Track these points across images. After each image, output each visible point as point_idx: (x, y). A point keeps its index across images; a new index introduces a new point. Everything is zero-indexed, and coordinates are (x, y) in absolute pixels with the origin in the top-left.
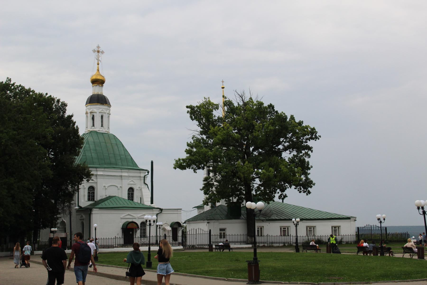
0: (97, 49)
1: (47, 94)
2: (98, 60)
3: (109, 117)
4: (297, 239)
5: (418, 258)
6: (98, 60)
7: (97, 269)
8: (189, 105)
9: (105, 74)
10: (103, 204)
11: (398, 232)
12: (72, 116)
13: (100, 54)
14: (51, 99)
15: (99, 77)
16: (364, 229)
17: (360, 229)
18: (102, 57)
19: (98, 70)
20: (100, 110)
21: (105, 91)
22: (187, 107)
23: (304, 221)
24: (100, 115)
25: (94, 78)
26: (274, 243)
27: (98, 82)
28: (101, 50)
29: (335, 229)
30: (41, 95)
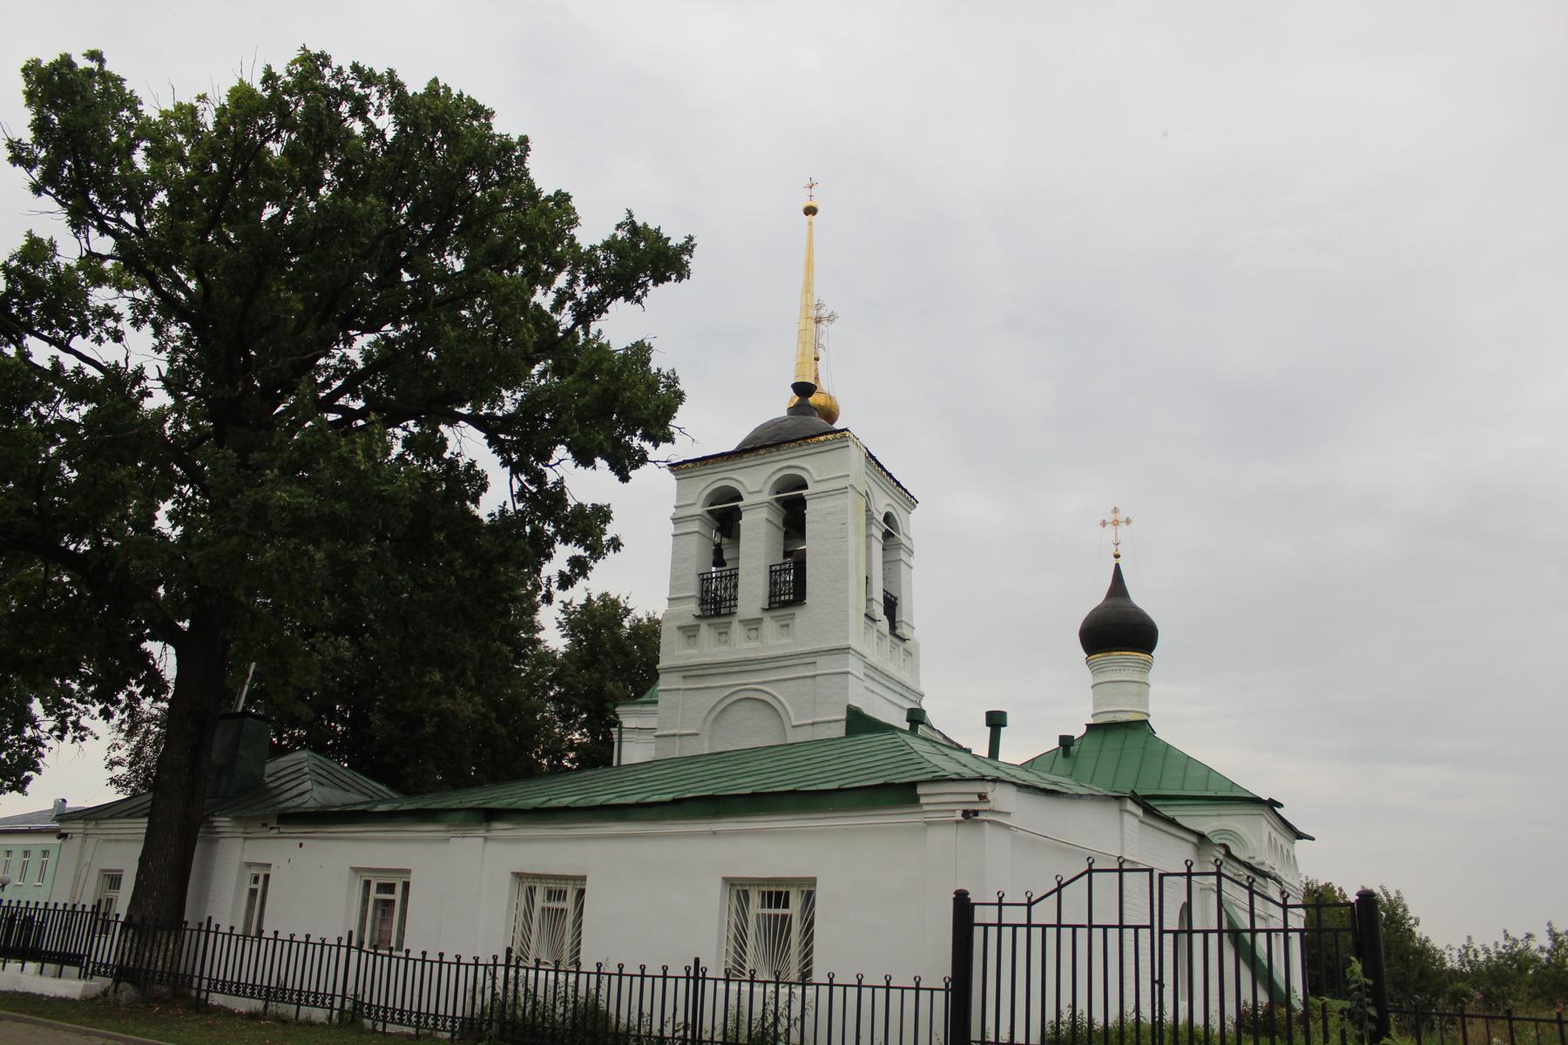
6: (817, 346)
13: (822, 327)
16: (1044, 913)
17: (980, 915)
23: (500, 829)
28: (824, 313)
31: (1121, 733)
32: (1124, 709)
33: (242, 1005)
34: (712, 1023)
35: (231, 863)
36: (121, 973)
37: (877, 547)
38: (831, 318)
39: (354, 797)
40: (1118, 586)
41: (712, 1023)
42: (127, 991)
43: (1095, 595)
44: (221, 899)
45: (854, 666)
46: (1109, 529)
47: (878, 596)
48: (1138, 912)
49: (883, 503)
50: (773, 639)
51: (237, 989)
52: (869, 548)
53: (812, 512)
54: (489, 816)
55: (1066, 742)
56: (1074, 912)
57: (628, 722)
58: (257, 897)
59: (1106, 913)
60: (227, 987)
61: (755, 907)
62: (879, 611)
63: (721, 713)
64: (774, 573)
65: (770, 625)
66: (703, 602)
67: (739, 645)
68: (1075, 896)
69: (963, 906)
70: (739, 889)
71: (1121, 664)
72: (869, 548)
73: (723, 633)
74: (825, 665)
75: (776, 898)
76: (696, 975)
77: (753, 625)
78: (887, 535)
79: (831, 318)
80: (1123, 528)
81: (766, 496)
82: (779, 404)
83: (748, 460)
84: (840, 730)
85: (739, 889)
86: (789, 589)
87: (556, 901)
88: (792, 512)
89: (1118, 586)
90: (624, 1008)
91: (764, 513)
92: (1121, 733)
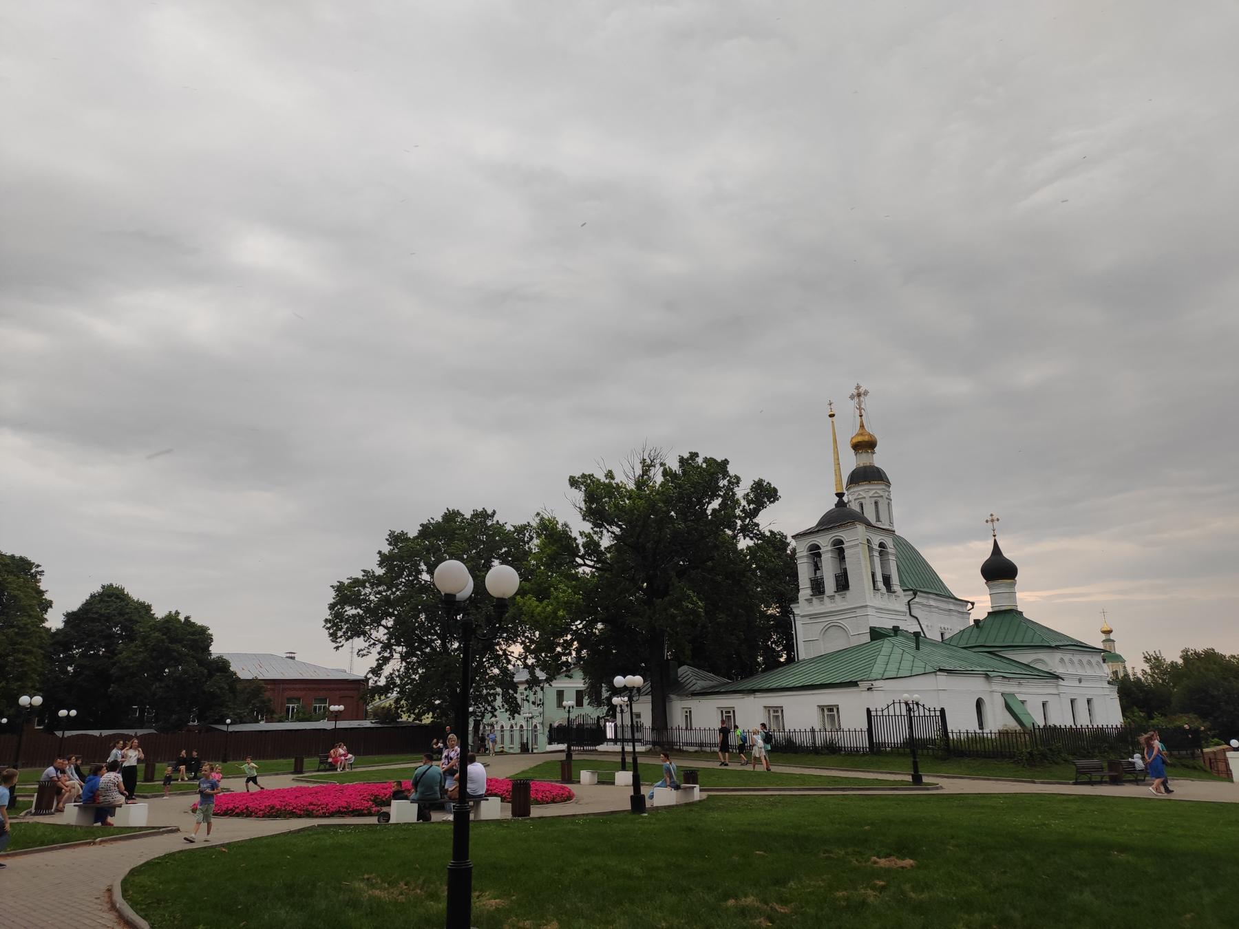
0: (855, 392)
1: (764, 494)
2: (860, 409)
3: (889, 504)
4: (814, 738)
5: (514, 814)
6: (860, 409)
7: (674, 792)
8: (577, 474)
9: (873, 429)
10: (1043, 655)
11: (410, 756)
12: (380, 552)
14: (451, 516)
15: (866, 438)
17: (873, 713)
18: (867, 402)
19: (862, 426)
20: (871, 493)
21: (879, 459)
22: (573, 482)
23: (758, 695)
24: (873, 500)
25: (855, 441)
26: (706, 745)
27: (865, 445)
28: (862, 390)
29: (830, 711)
30: (13, 557)
31: (1005, 616)
32: (1005, 605)
33: (692, 749)
34: (818, 743)
35: (678, 708)
36: (654, 743)
37: (877, 560)
38: (866, 393)
39: (712, 683)
40: (996, 550)
41: (818, 743)
42: (658, 748)
43: (987, 555)
44: (677, 718)
45: (870, 611)
46: (990, 524)
47: (879, 578)
48: (904, 713)
49: (876, 540)
50: (840, 603)
51: (691, 744)
52: (871, 557)
53: (847, 553)
54: (753, 691)
55: (977, 622)
56: (892, 713)
57: (796, 611)
58: (688, 716)
59: (898, 713)
60: (687, 744)
61: (826, 712)
62: (880, 585)
63: (825, 631)
64: (837, 577)
65: (838, 597)
66: (812, 589)
67: (828, 606)
68: (891, 708)
69: (869, 711)
70: (822, 708)
71: (1002, 586)
72: (871, 557)
73: (822, 600)
74: (859, 612)
75: (831, 710)
76: (813, 731)
77: (831, 597)
78: (881, 553)
79: (866, 393)
80: (996, 523)
81: (829, 548)
82: (831, 503)
83: (821, 534)
84: (867, 638)
85: (822, 708)
86: (843, 583)
87: (776, 713)
88: (839, 550)
89: (996, 550)
90: (798, 740)
91: (830, 555)
92: (1005, 616)
